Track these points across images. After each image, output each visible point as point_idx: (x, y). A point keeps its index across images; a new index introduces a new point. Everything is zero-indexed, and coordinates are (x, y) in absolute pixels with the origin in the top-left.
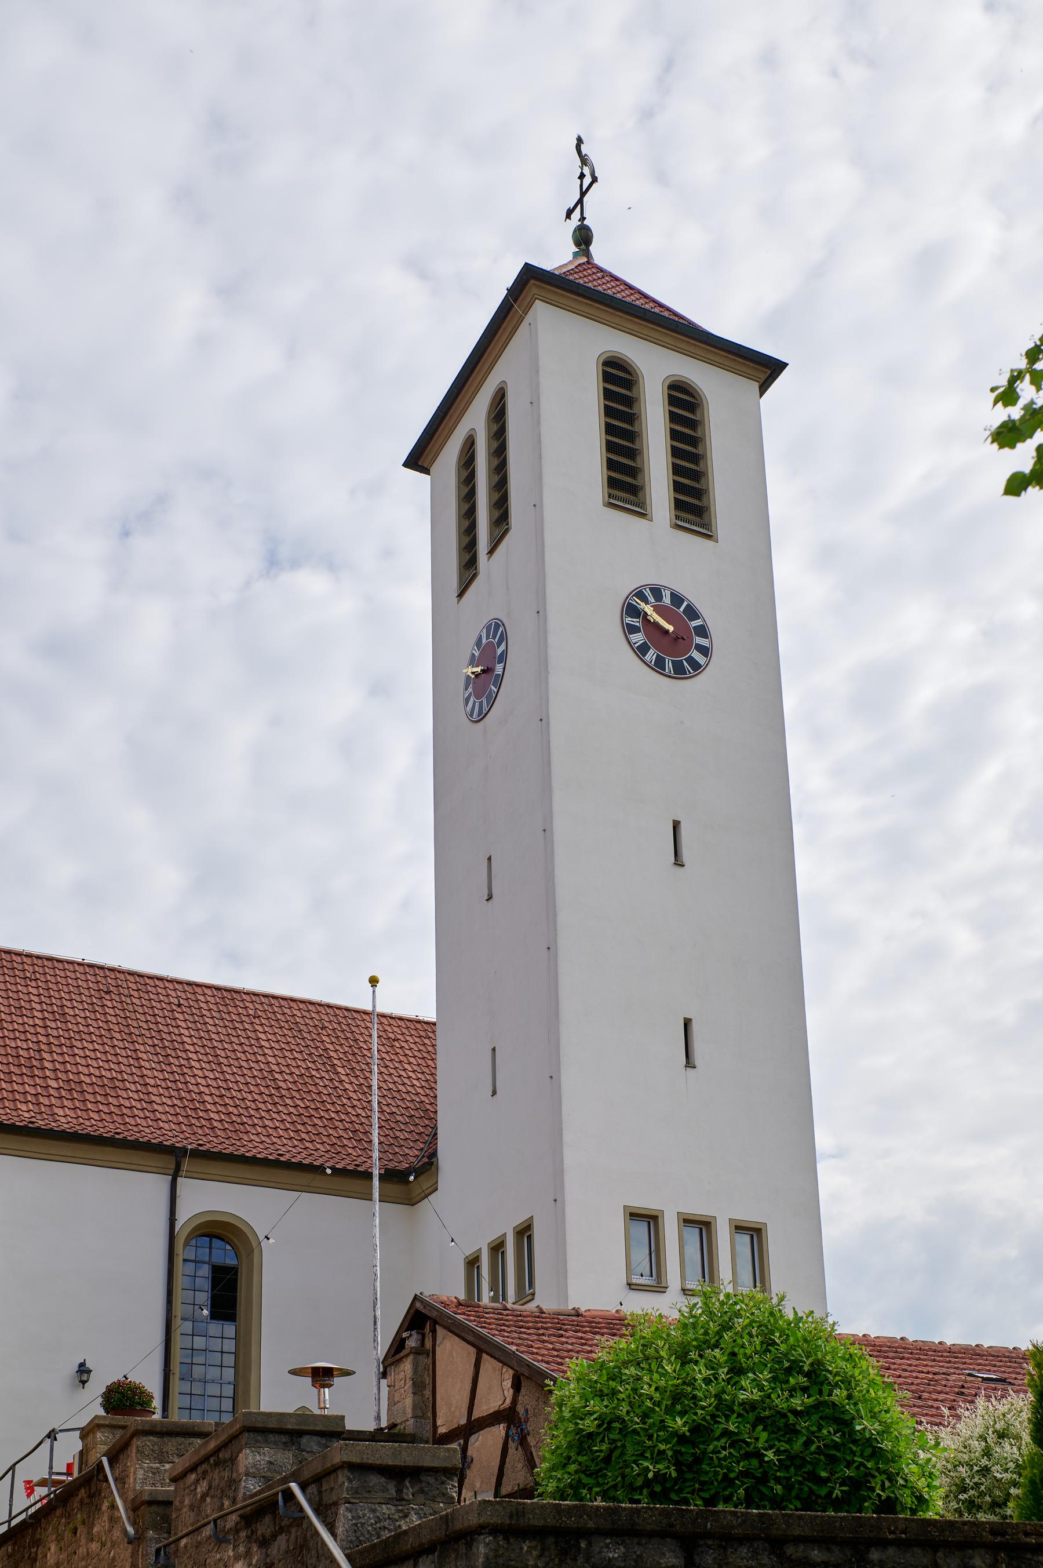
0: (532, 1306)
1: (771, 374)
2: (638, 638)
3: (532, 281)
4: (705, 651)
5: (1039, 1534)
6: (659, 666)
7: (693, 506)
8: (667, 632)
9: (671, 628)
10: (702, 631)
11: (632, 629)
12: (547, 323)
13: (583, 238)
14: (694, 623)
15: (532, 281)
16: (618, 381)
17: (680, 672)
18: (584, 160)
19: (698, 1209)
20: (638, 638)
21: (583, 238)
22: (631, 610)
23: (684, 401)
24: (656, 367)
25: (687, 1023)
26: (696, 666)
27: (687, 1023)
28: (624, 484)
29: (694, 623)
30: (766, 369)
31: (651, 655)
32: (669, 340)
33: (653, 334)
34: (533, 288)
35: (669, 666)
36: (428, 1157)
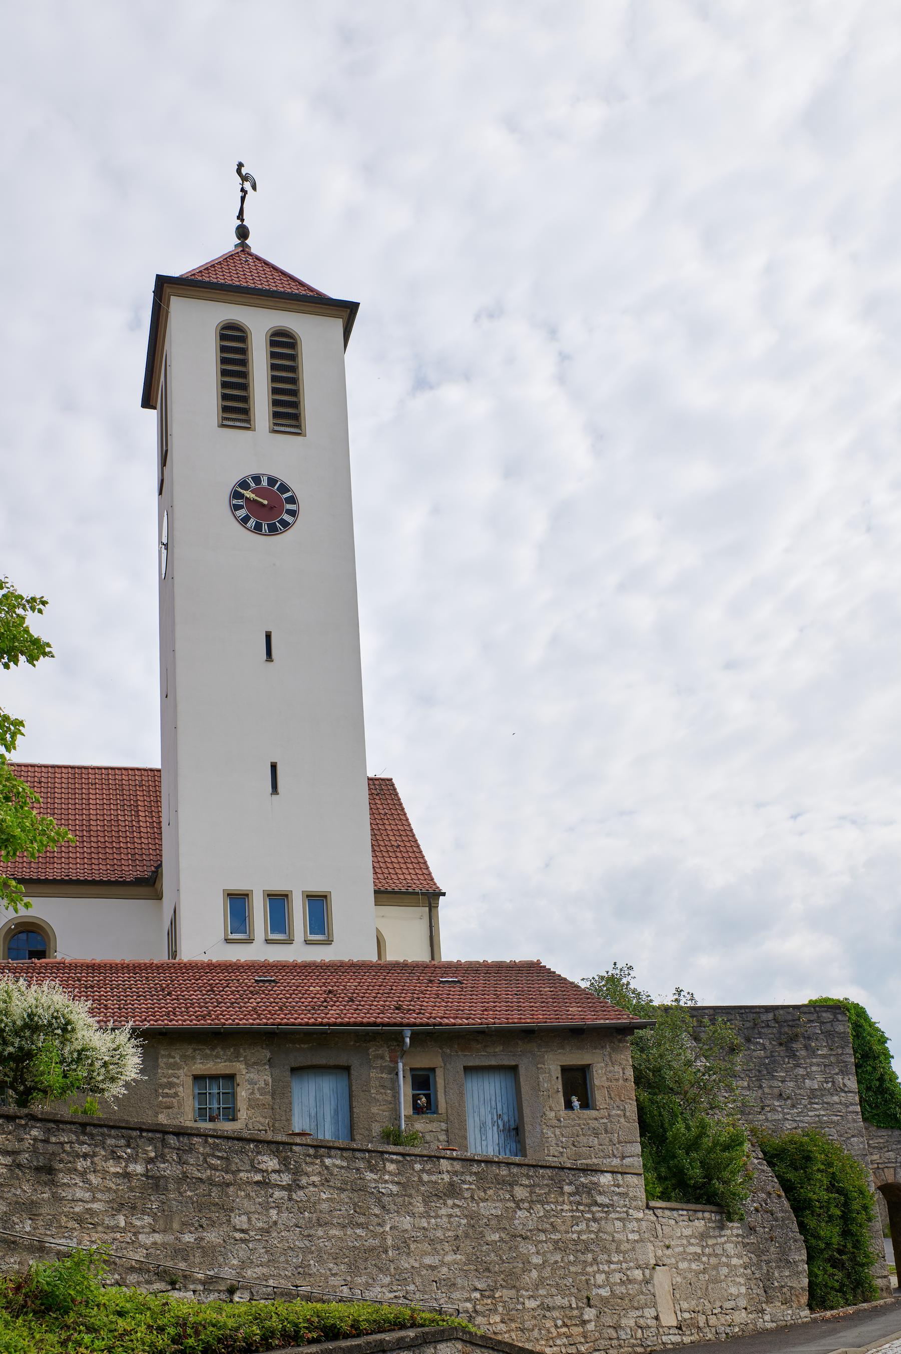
0: (177, 960)
1: (351, 311)
2: (242, 513)
3: (165, 285)
4: (293, 513)
5: (899, 1142)
6: (258, 528)
7: (288, 414)
8: (264, 505)
9: (266, 502)
10: (292, 500)
11: (237, 507)
12: (181, 309)
13: (243, 233)
14: (285, 496)
15: (165, 285)
16: (233, 339)
17: (273, 530)
18: (245, 178)
19: (278, 886)
20: (242, 513)
21: (243, 233)
22: (236, 495)
23: (284, 346)
24: (260, 323)
25: (274, 767)
26: (285, 524)
27: (274, 767)
28: (235, 408)
29: (285, 496)
30: (347, 311)
31: (252, 523)
32: (270, 303)
33: (258, 301)
34: (167, 289)
35: (265, 527)
36: (156, 867)
